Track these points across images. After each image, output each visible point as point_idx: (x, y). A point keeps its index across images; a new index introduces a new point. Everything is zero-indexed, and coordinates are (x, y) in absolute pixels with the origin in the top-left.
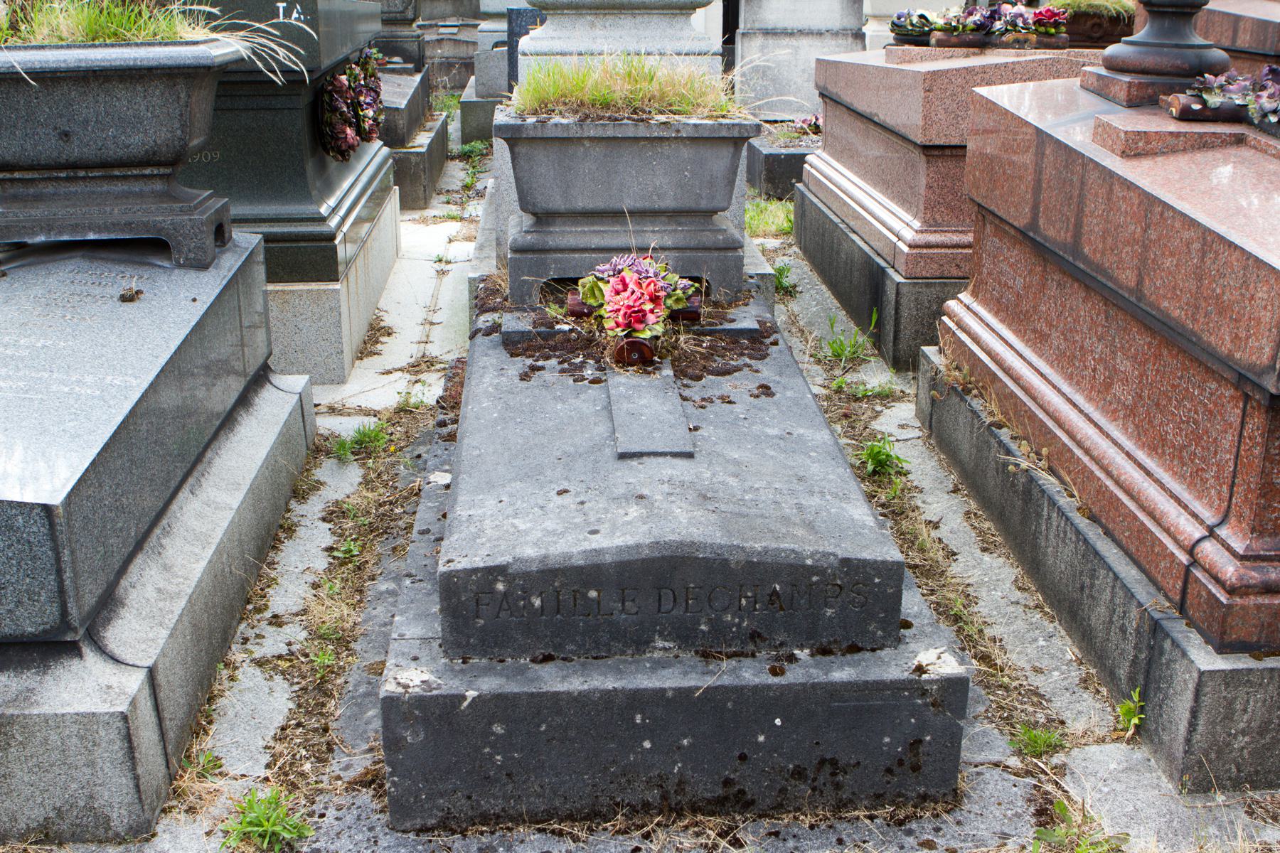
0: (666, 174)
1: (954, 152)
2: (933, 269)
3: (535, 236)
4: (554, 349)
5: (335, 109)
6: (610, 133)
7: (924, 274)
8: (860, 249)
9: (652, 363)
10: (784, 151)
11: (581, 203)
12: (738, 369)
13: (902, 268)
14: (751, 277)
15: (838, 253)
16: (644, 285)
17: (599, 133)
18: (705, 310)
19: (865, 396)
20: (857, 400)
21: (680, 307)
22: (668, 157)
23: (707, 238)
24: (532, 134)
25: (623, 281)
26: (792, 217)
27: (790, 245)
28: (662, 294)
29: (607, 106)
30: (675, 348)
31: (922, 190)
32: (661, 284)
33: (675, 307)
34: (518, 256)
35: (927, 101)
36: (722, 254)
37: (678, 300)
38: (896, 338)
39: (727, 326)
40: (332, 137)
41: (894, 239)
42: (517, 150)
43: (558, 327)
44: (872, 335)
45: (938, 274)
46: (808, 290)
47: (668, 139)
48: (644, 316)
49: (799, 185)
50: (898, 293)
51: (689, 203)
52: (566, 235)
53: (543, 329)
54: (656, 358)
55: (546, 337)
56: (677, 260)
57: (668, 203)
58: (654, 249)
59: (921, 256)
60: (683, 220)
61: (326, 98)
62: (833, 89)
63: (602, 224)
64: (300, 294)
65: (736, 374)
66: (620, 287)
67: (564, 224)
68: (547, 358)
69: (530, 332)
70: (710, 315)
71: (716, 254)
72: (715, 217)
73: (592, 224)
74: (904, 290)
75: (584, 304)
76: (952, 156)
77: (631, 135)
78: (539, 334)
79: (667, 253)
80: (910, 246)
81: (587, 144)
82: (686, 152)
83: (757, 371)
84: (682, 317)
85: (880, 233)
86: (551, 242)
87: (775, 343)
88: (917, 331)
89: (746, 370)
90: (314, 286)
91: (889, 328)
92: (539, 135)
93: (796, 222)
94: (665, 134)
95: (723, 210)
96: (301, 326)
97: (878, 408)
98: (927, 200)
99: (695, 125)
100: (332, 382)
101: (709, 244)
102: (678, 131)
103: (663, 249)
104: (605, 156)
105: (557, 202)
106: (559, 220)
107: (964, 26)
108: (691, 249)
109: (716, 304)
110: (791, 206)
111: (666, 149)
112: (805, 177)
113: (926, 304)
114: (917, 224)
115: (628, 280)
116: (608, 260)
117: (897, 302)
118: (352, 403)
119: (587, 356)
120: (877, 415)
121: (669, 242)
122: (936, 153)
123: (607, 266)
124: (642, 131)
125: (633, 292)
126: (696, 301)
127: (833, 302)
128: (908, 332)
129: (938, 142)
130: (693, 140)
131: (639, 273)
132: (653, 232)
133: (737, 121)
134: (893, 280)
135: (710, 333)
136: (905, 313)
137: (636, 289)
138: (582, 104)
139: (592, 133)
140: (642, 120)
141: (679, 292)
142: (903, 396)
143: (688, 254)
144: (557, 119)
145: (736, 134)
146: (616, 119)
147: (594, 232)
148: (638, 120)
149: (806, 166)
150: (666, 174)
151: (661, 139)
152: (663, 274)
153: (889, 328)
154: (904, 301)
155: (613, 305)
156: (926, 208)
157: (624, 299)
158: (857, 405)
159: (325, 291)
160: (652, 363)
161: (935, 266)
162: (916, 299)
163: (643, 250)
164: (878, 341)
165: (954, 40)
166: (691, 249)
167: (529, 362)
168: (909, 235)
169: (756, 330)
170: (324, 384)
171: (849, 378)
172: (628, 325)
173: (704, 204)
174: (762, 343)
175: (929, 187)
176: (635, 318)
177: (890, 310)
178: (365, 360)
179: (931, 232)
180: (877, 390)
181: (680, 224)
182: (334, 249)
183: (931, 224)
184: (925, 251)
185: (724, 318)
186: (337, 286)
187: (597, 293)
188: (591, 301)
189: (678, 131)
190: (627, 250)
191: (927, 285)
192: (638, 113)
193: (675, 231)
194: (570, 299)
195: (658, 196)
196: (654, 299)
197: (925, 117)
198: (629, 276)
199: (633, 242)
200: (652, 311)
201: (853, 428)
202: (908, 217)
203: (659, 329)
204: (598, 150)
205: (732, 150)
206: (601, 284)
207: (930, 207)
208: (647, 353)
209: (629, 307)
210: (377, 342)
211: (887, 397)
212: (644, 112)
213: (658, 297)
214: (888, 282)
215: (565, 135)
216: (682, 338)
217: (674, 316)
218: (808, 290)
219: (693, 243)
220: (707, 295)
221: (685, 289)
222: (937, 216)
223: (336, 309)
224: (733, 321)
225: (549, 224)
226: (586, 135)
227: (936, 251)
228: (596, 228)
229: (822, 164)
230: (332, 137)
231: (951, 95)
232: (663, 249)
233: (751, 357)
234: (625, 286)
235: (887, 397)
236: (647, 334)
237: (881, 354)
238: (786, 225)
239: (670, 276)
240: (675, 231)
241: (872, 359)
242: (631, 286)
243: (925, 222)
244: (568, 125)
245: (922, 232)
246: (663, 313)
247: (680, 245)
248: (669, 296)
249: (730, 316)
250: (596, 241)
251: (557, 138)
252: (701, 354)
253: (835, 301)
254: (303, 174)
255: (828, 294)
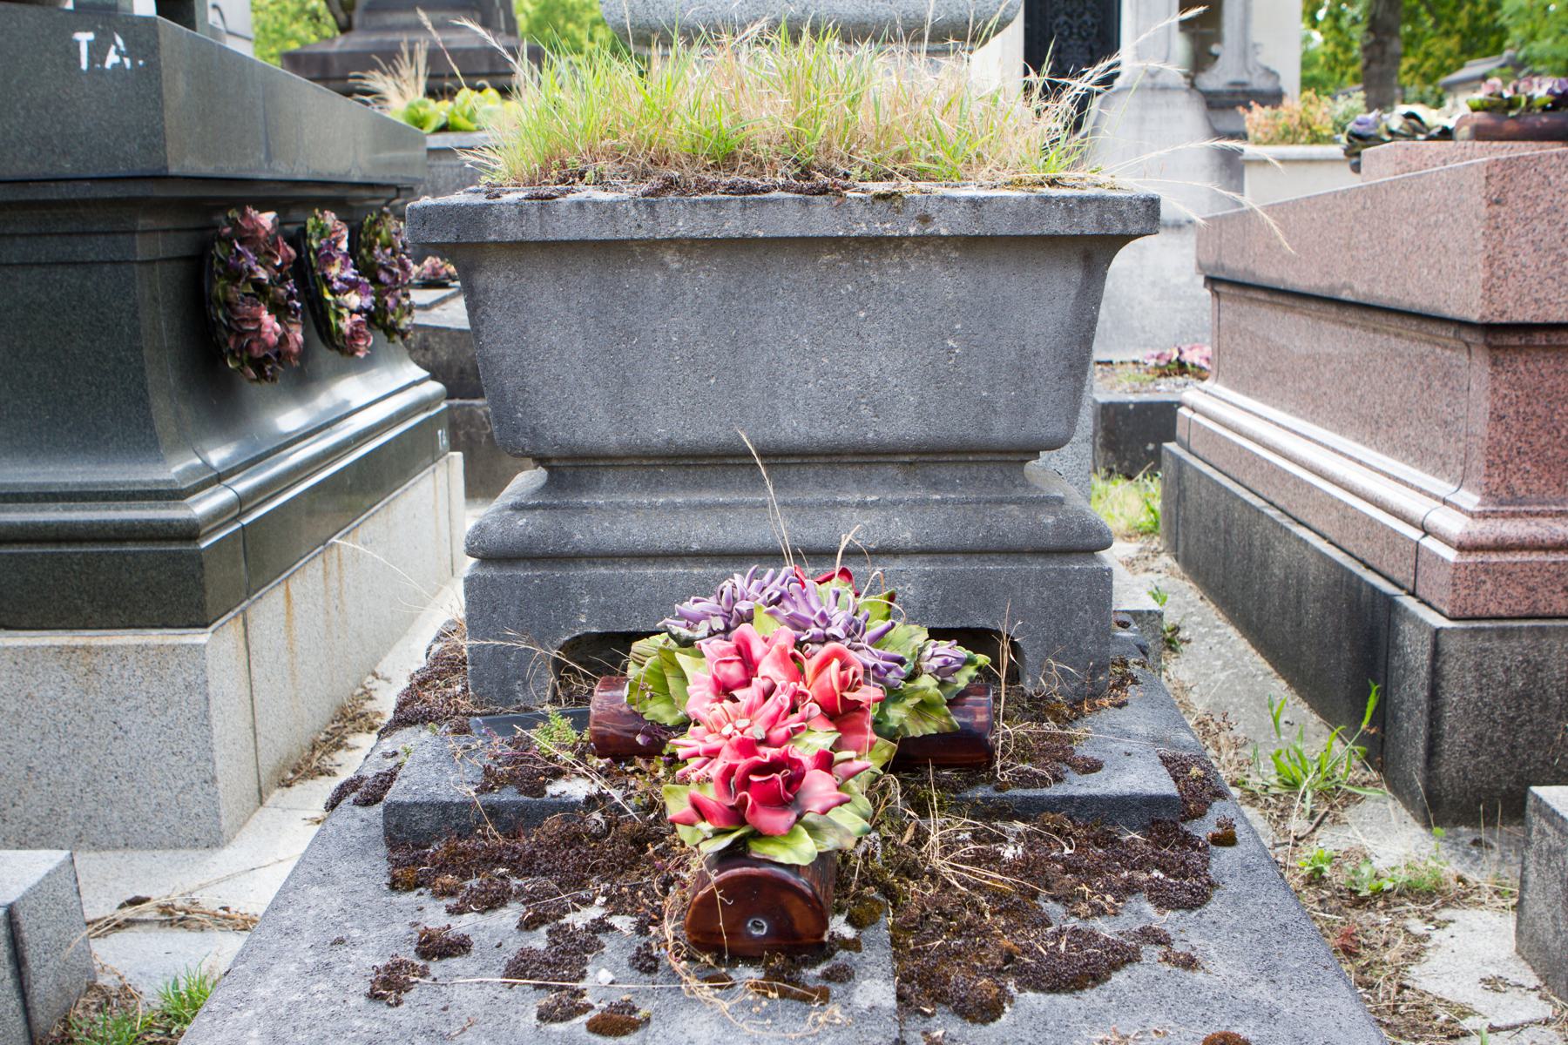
0: (893, 344)
1: (1554, 338)
2: (1513, 598)
3: (539, 518)
4: (525, 866)
5: (235, 275)
6: (732, 226)
7: (1493, 608)
8: (1322, 556)
9: (820, 950)
10: (1133, 398)
11: (665, 426)
12: (1121, 957)
13: (1442, 596)
14: (1124, 625)
15: (1264, 565)
16: (810, 666)
17: (703, 225)
18: (1007, 732)
19: (1380, 893)
20: (1360, 902)
21: (931, 728)
22: (901, 298)
23: (1011, 522)
24: (513, 232)
25: (744, 653)
26: (1157, 504)
27: (1156, 553)
28: (868, 693)
29: (728, 160)
30: (910, 871)
31: (1480, 425)
32: (866, 657)
33: (916, 730)
34: (491, 572)
35: (1494, 225)
36: (1053, 565)
37: (924, 708)
38: (1432, 751)
39: (1079, 786)
40: (230, 330)
41: (1415, 534)
42: (480, 280)
43: (554, 789)
44: (1364, 739)
45: (1523, 608)
46: (1203, 637)
47: (897, 242)
48: (795, 780)
49: (1171, 446)
50: (1436, 653)
51: (957, 425)
52: (622, 516)
53: (509, 795)
54: (839, 926)
55: (512, 822)
56: (930, 581)
57: (903, 426)
58: (851, 553)
59: (1487, 569)
60: (944, 473)
61: (219, 251)
62: (1236, 265)
63: (726, 487)
64: (122, 655)
65: (1119, 979)
66: (734, 671)
67: (622, 486)
68: (492, 902)
69: (466, 805)
70: (1024, 751)
71: (1036, 565)
72: (1032, 466)
73: (698, 486)
74: (1450, 645)
75: (638, 716)
76: (1546, 348)
77: (791, 231)
78: (494, 811)
79: (899, 564)
80: (1461, 548)
81: (671, 259)
82: (948, 282)
83: (1190, 963)
84: (938, 763)
85: (1372, 521)
86: (582, 533)
87: (1226, 839)
88: (1479, 737)
89: (1152, 953)
90: (155, 637)
91: (1413, 727)
92: (535, 234)
93: (1166, 512)
94: (889, 229)
95: (1055, 445)
96: (125, 723)
97: (1417, 926)
98: (1494, 446)
99: (974, 203)
100: (195, 843)
101: (1018, 539)
102: (925, 219)
103: (885, 552)
104: (725, 295)
105: (597, 427)
106: (608, 477)
107: (1530, 99)
108: (968, 552)
109: (1038, 708)
110: (1155, 487)
111: (893, 274)
112: (1180, 431)
113: (1501, 676)
114: (1471, 499)
115: (757, 650)
116: (705, 589)
117: (1435, 673)
118: (210, 900)
119: (616, 904)
120: (1418, 949)
121: (904, 532)
122: (1514, 340)
123: (709, 604)
124: (823, 220)
125: (767, 694)
126: (978, 713)
127: (1257, 663)
128: (1459, 739)
129: (1518, 317)
130: (972, 245)
131: (797, 623)
132: (863, 505)
133: (1091, 192)
134: (1420, 623)
135: (1025, 810)
136: (1451, 695)
137: (781, 679)
138: (663, 159)
139: (682, 228)
140: (824, 191)
141: (926, 682)
142: (1464, 896)
143: (960, 566)
144: (587, 192)
145: (1090, 228)
146: (750, 190)
147: (702, 506)
148: (812, 191)
149: (1182, 411)
150: (893, 344)
151: (877, 244)
152: (878, 626)
153: (1413, 727)
154: (1450, 668)
155: (712, 728)
156: (1490, 464)
157: (745, 718)
158: (1362, 917)
159: (174, 648)
160: (820, 950)
161: (1517, 592)
162: (1478, 667)
163: (818, 555)
164: (1380, 753)
165: (1510, 126)
166: (968, 552)
167: (436, 915)
168: (1456, 525)
169: (1166, 800)
170: (177, 846)
171: (1328, 841)
172: (736, 815)
173: (1001, 430)
174: (1188, 841)
175: (1497, 417)
176: (769, 783)
177: (1415, 688)
178: (297, 787)
179: (1504, 516)
180: (1403, 876)
181: (935, 486)
182: (1104, 579)
183: (1502, 501)
184: (1494, 558)
185: (1063, 758)
186: (200, 637)
187: (672, 683)
188: (657, 711)
189: (925, 219)
190: (772, 556)
191: (1503, 634)
192: (813, 180)
193: (924, 503)
194: (601, 699)
195: (876, 407)
196: (841, 713)
197: (1490, 261)
198: (768, 635)
199: (781, 530)
200: (825, 761)
201: (1370, 986)
202: (1443, 487)
203: (849, 824)
204: (705, 280)
205: (1076, 275)
206: (683, 659)
207: (1499, 460)
208: (801, 919)
209: (747, 747)
210: (338, 746)
211: (1429, 895)
212: (829, 171)
213: (856, 706)
214: (1407, 628)
215: (607, 234)
216: (936, 829)
217: (909, 758)
218: (1203, 637)
219: (972, 537)
220: (1014, 676)
221: (944, 673)
222: (1516, 482)
223: (199, 688)
224: (1093, 767)
225: (579, 488)
226: (663, 234)
227: (1518, 557)
228: (708, 497)
229: (1210, 404)
230: (230, 330)
231: (1547, 211)
232: (885, 552)
233: (1163, 899)
234: (750, 666)
235: (1429, 895)
236: (801, 851)
237: (1399, 787)
238: (1145, 520)
239: (901, 630)
240: (924, 503)
241: (1368, 792)
242: (768, 669)
243: (1489, 494)
244: (613, 205)
245: (1484, 516)
246: (869, 757)
247: (937, 541)
248: (894, 695)
249: (1083, 751)
250: (703, 532)
251: (583, 243)
252: (997, 896)
253: (1259, 659)
254: (141, 400)
255: (1243, 644)
